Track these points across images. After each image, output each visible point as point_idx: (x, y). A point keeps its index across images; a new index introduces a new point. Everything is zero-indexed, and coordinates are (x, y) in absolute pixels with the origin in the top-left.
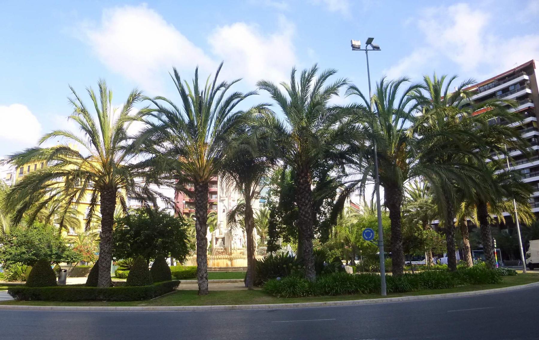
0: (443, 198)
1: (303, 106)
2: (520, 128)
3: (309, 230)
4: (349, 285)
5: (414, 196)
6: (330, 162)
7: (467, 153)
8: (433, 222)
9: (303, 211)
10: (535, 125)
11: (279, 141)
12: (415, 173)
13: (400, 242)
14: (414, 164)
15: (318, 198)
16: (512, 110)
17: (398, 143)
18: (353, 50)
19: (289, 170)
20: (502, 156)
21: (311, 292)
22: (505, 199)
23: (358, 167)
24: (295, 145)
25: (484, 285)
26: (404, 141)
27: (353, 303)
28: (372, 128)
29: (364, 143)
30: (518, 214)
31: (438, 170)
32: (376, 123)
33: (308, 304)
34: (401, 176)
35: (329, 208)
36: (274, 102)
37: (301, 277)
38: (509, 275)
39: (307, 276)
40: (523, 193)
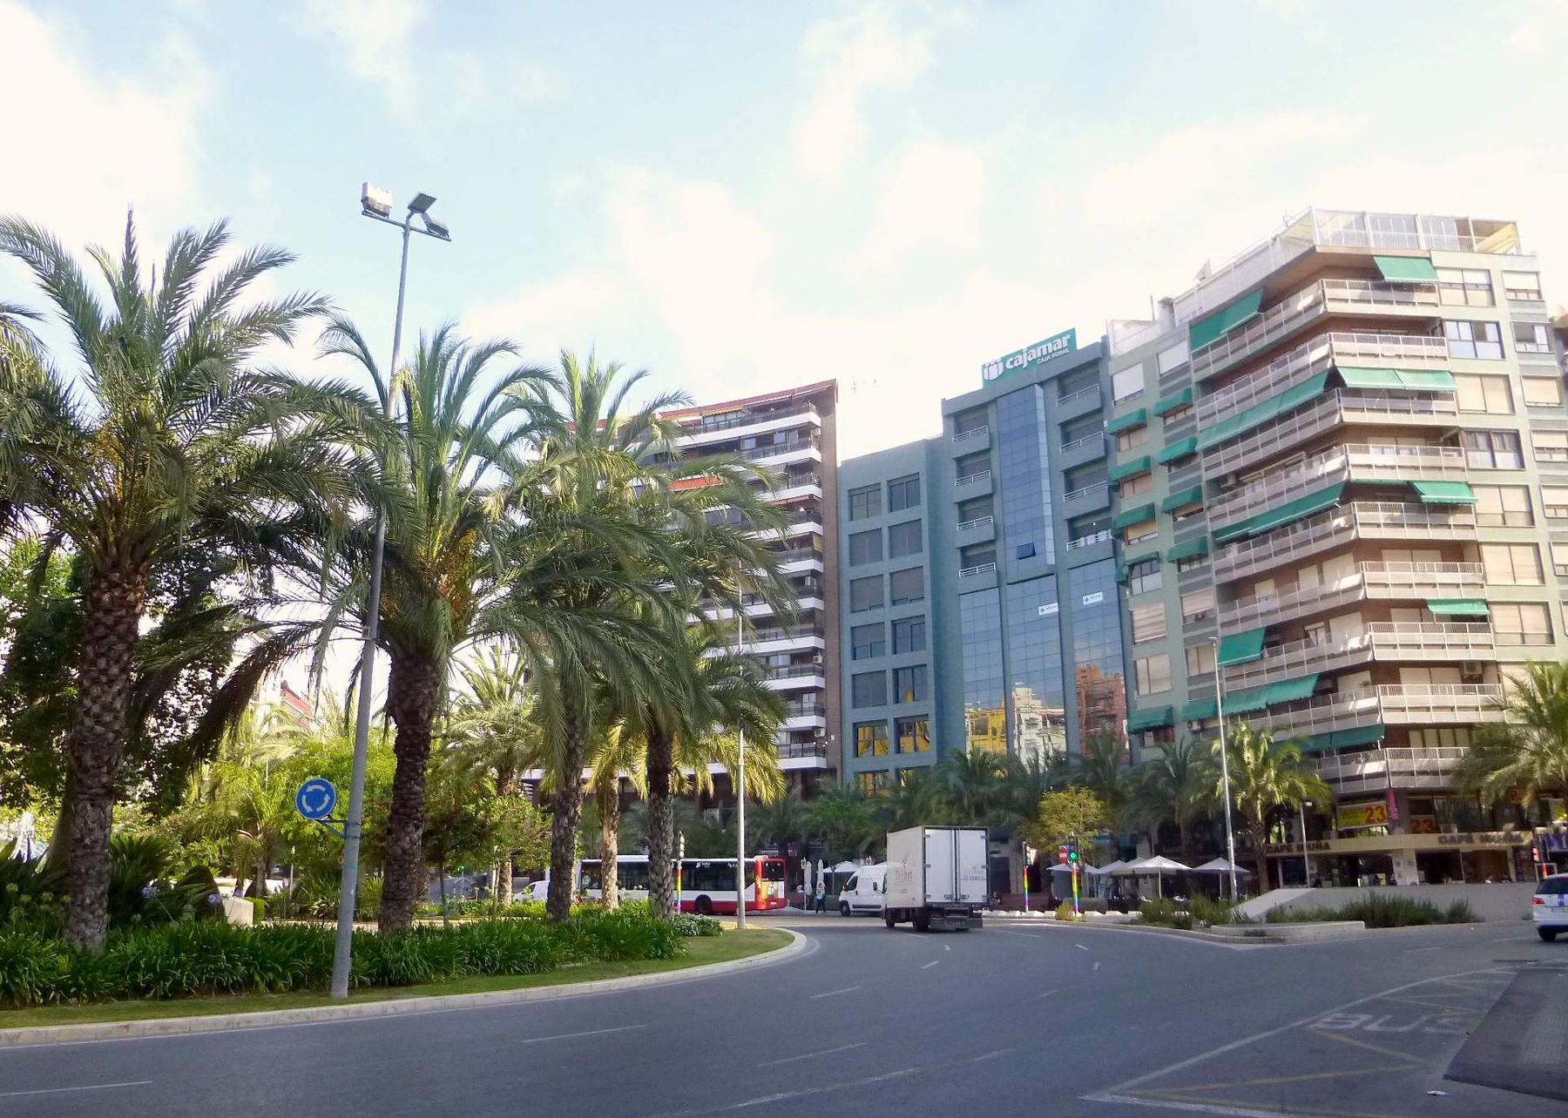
0: (558, 709)
1: (157, 348)
2: (776, 546)
3: (105, 769)
4: (222, 965)
5: (484, 691)
6: (227, 550)
7: (639, 591)
8: (526, 775)
9: (94, 701)
10: (817, 545)
11: (45, 447)
12: (492, 627)
13: (417, 828)
14: (493, 597)
15: (164, 662)
16: (768, 497)
17: (455, 529)
18: (365, 213)
19: (66, 552)
20: (728, 613)
21: (79, 987)
22: (718, 728)
23: (317, 580)
24: (102, 471)
25: (634, 963)
26: (472, 526)
27: (228, 1024)
28: (383, 467)
29: (346, 508)
30: (747, 773)
31: (557, 627)
32: (397, 458)
33: (59, 1033)
34: (445, 629)
35: (197, 700)
36: (49, 306)
37: (49, 935)
38: (703, 934)
39: (72, 931)
40: (765, 718)
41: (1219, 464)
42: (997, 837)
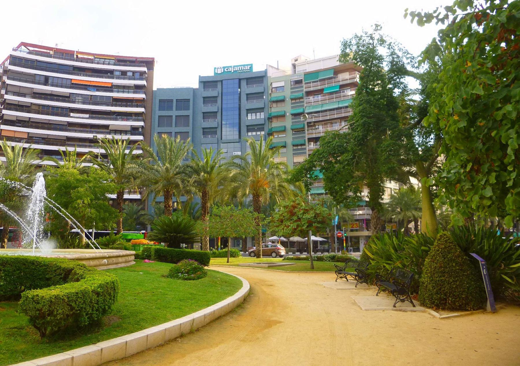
41: (327, 116)
42: (496, 183)
